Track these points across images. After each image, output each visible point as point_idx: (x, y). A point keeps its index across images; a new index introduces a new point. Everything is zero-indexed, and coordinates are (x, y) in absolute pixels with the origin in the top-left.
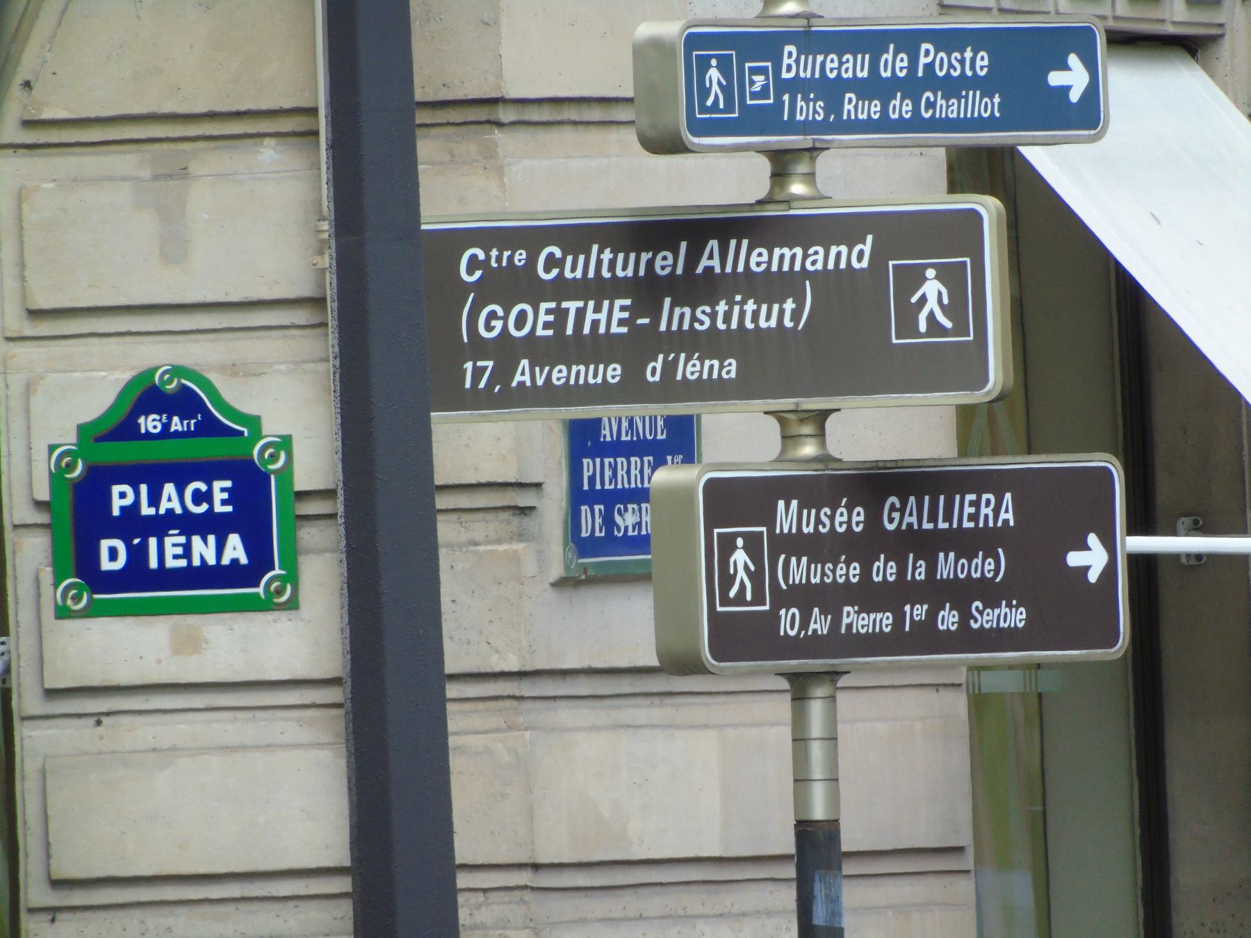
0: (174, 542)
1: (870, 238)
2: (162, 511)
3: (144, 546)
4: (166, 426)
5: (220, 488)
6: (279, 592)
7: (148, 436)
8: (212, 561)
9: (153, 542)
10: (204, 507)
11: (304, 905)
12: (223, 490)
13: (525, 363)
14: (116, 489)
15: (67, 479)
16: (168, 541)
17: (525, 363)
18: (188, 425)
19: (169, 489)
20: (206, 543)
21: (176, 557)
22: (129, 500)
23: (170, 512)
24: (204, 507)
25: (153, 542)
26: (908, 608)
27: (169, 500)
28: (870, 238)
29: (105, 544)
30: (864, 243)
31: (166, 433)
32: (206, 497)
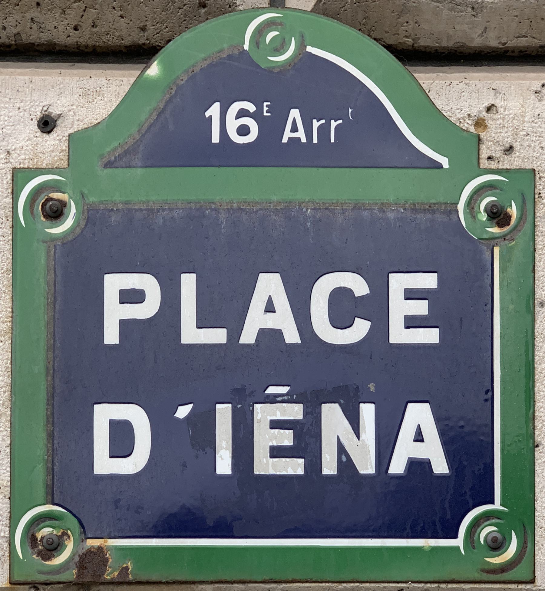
0: (272, 418)
2: (248, 336)
4: (271, 127)
5: (407, 293)
6: (497, 545)
7: (228, 154)
9: (224, 413)
12: (411, 295)
14: (114, 283)
15: (53, 239)
18: (324, 131)
19: (270, 285)
20: (341, 449)
21: (277, 452)
22: (148, 309)
23: (270, 337)
25: (224, 413)
26: (214, 111)
27: (270, 308)
28: (111, 336)
30: (124, 324)
31: (269, 150)
32: (376, 308)
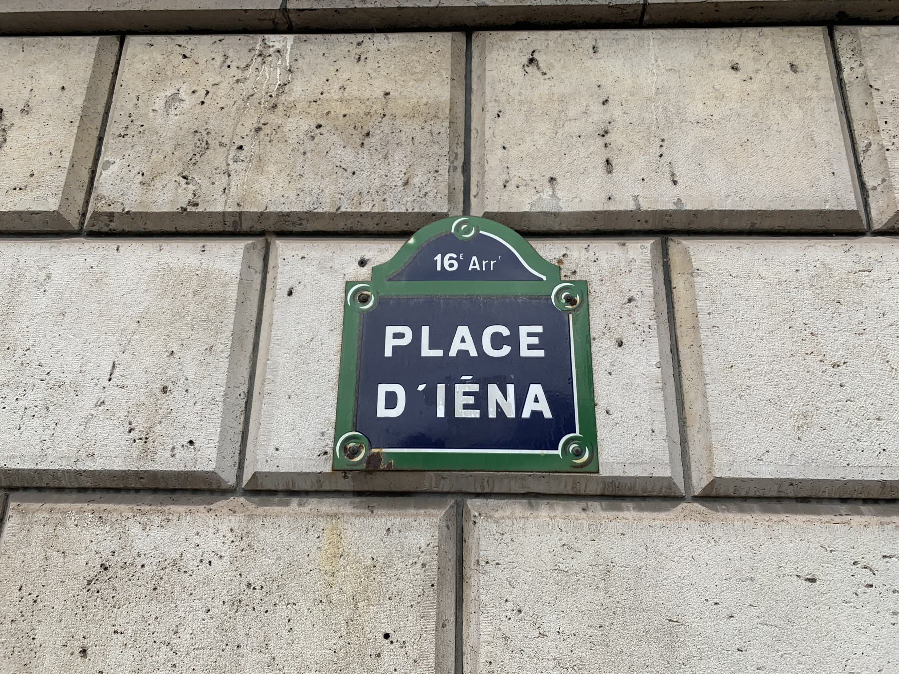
1: (388, 353)
2: (453, 353)
3: (431, 394)
5: (528, 337)
6: (579, 454)
8: (511, 413)
9: (441, 389)
10: (506, 350)
11: (470, 640)
13: (475, 258)
14: (390, 330)
16: (460, 389)
17: (475, 258)
18: (488, 265)
20: (498, 406)
21: (466, 407)
22: (406, 341)
24: (506, 350)
25: (441, 389)
28: (388, 353)
29: (383, 389)
31: (464, 273)
32: (514, 340)
